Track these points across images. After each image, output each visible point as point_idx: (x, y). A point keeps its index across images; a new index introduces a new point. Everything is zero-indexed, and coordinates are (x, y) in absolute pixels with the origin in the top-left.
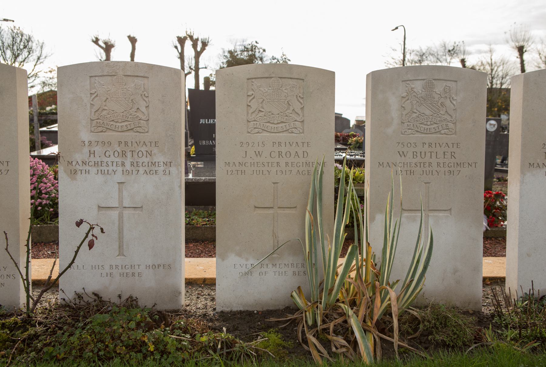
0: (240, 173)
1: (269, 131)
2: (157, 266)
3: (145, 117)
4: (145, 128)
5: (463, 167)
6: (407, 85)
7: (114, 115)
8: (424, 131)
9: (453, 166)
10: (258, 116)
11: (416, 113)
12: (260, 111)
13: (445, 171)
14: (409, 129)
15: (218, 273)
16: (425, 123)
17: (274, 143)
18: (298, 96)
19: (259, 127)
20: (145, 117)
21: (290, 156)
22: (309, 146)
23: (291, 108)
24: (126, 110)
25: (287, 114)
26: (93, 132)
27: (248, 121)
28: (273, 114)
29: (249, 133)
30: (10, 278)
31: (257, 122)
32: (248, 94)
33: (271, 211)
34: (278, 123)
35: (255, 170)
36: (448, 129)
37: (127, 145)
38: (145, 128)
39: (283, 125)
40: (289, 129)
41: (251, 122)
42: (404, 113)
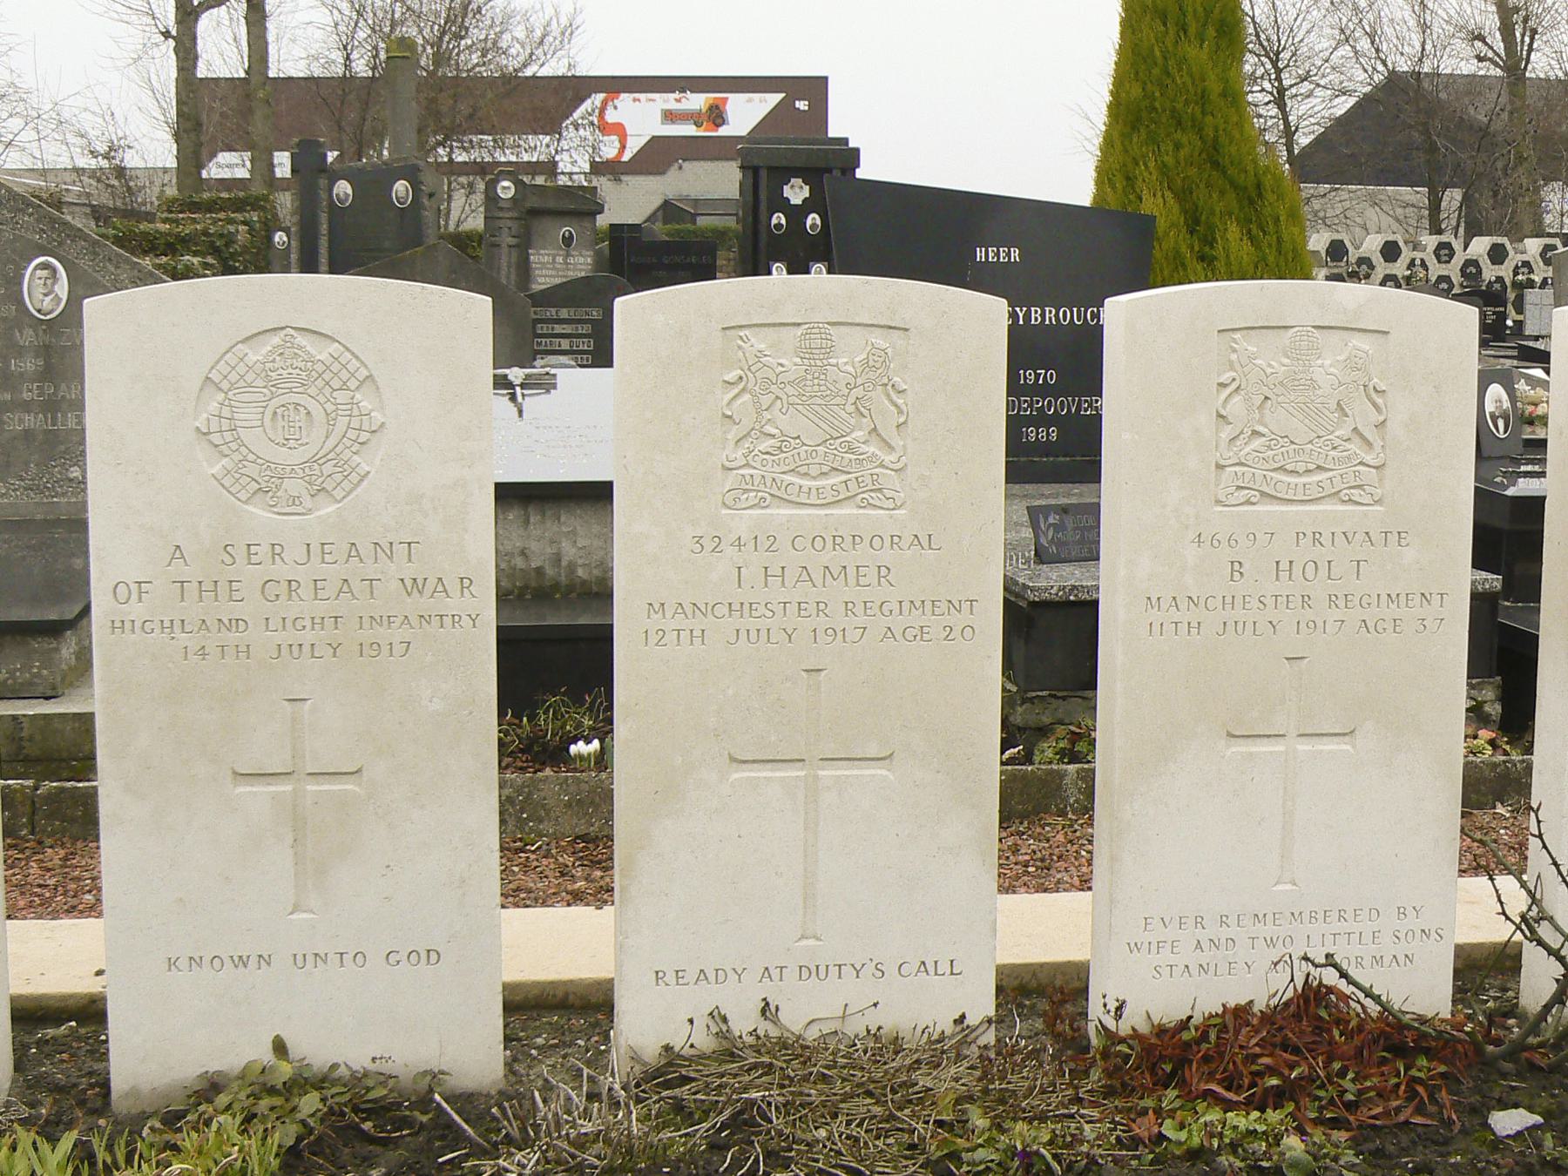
1: (1279, 495)
2: (424, 955)
3: (893, 457)
4: (1372, 490)
8: (798, 496)
9: (308, 628)
10: (1247, 449)
15: (619, 965)
16: (803, 469)
18: (1371, 387)
20: (893, 457)
21: (116, 586)
22: (1403, 542)
23: (1349, 425)
24: (835, 434)
25: (1337, 442)
27: (1219, 467)
28: (1292, 442)
29: (1218, 502)
31: (1246, 469)
37: (1320, 543)
38: (1372, 490)
40: (1340, 491)
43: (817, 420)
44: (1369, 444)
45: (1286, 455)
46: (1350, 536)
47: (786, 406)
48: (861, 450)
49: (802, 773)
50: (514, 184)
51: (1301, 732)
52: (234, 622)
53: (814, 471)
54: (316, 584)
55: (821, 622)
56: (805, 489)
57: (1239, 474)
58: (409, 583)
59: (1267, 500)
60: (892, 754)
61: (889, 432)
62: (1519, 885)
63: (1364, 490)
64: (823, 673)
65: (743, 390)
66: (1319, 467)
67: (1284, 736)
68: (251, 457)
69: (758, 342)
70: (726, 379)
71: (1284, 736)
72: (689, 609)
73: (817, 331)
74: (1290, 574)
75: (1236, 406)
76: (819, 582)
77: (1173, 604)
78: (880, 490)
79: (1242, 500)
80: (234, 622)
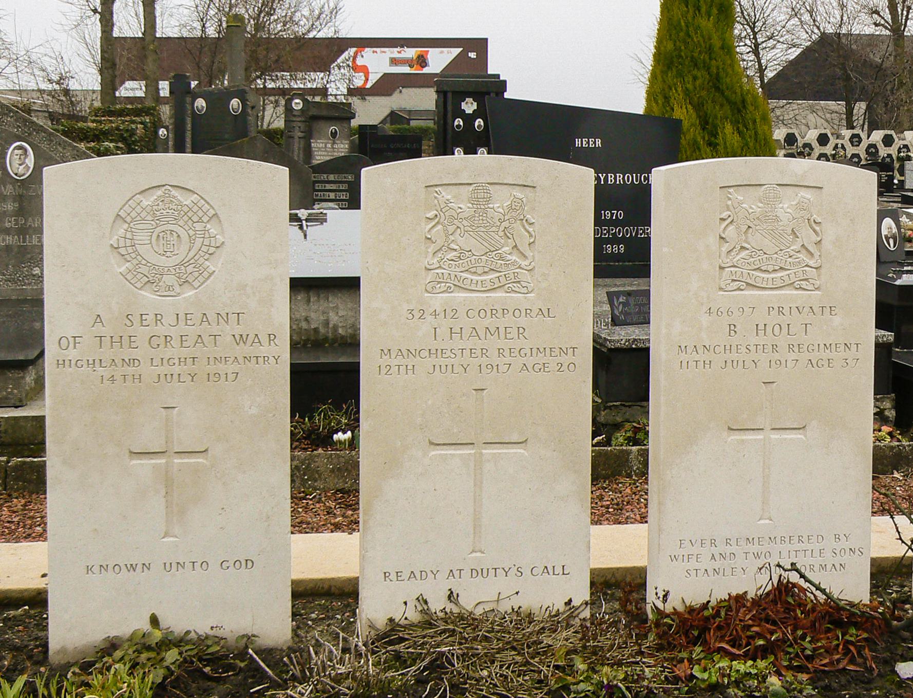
0: (701, 364)
1: (757, 285)
5: (836, 351)
6: (729, 196)
7: (759, 257)
9: (177, 364)
10: (738, 258)
11: (748, 249)
12: (742, 248)
13: (380, 366)
14: (733, 280)
16: (473, 270)
17: (771, 309)
18: (812, 220)
19: (740, 279)
20: (527, 263)
21: (60, 339)
25: (792, 253)
26: (430, 293)
27: (721, 268)
28: (765, 253)
29: (721, 289)
30: (854, 554)
32: (721, 217)
33: (759, 436)
34: (775, 270)
35: (742, 360)
36: (519, 282)
37: (782, 313)
39: (493, 275)
41: (727, 269)
42: (725, 248)
43: (481, 241)
44: (812, 254)
45: (469, 262)
46: (801, 310)
47: (463, 232)
48: (507, 259)
49: (473, 452)
50: (302, 101)
51: (773, 427)
52: (132, 361)
53: (480, 271)
54: (182, 338)
55: (484, 361)
56: (474, 282)
57: (733, 272)
58: (238, 337)
59: (751, 288)
60: (526, 440)
61: (524, 248)
62: (909, 521)
63: (809, 282)
64: (485, 391)
65: (438, 223)
66: (781, 268)
67: (763, 429)
68: (144, 262)
69: (446, 194)
70: (427, 216)
71: (763, 429)
72: (405, 353)
73: (481, 188)
74: (765, 332)
75: (731, 232)
76: (483, 337)
77: (695, 350)
78: (519, 282)
79: (735, 288)
80: (132, 361)
